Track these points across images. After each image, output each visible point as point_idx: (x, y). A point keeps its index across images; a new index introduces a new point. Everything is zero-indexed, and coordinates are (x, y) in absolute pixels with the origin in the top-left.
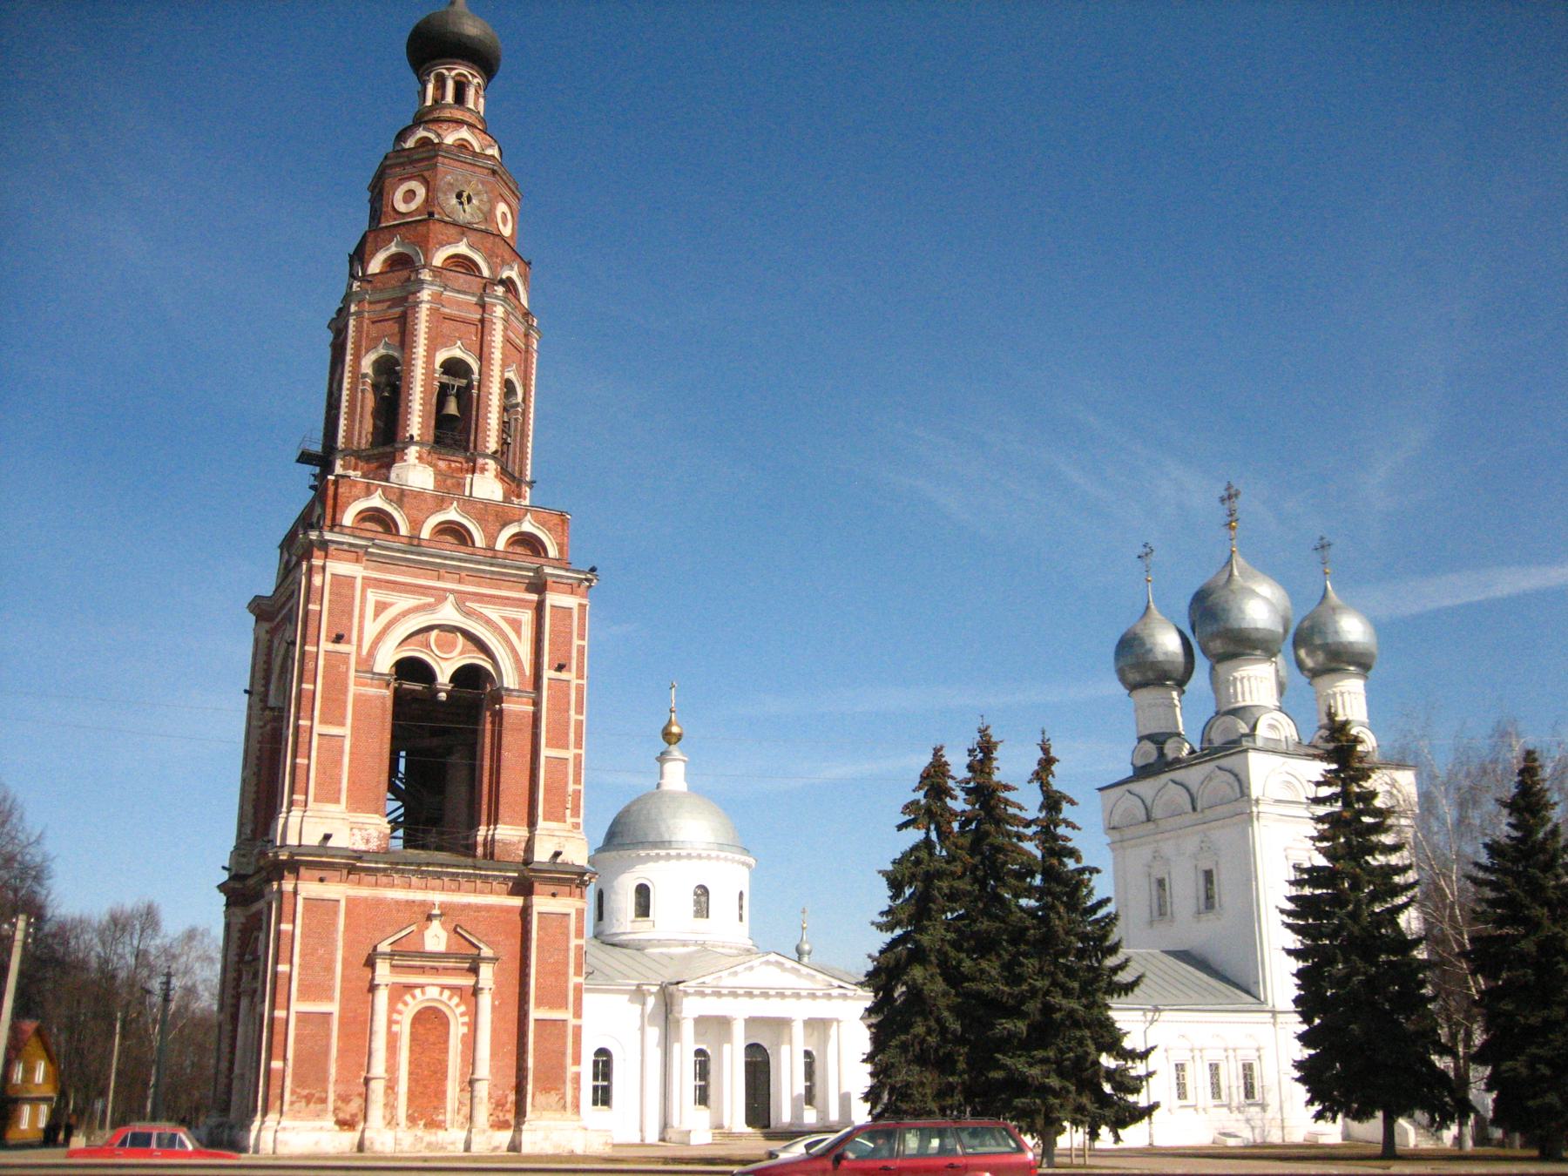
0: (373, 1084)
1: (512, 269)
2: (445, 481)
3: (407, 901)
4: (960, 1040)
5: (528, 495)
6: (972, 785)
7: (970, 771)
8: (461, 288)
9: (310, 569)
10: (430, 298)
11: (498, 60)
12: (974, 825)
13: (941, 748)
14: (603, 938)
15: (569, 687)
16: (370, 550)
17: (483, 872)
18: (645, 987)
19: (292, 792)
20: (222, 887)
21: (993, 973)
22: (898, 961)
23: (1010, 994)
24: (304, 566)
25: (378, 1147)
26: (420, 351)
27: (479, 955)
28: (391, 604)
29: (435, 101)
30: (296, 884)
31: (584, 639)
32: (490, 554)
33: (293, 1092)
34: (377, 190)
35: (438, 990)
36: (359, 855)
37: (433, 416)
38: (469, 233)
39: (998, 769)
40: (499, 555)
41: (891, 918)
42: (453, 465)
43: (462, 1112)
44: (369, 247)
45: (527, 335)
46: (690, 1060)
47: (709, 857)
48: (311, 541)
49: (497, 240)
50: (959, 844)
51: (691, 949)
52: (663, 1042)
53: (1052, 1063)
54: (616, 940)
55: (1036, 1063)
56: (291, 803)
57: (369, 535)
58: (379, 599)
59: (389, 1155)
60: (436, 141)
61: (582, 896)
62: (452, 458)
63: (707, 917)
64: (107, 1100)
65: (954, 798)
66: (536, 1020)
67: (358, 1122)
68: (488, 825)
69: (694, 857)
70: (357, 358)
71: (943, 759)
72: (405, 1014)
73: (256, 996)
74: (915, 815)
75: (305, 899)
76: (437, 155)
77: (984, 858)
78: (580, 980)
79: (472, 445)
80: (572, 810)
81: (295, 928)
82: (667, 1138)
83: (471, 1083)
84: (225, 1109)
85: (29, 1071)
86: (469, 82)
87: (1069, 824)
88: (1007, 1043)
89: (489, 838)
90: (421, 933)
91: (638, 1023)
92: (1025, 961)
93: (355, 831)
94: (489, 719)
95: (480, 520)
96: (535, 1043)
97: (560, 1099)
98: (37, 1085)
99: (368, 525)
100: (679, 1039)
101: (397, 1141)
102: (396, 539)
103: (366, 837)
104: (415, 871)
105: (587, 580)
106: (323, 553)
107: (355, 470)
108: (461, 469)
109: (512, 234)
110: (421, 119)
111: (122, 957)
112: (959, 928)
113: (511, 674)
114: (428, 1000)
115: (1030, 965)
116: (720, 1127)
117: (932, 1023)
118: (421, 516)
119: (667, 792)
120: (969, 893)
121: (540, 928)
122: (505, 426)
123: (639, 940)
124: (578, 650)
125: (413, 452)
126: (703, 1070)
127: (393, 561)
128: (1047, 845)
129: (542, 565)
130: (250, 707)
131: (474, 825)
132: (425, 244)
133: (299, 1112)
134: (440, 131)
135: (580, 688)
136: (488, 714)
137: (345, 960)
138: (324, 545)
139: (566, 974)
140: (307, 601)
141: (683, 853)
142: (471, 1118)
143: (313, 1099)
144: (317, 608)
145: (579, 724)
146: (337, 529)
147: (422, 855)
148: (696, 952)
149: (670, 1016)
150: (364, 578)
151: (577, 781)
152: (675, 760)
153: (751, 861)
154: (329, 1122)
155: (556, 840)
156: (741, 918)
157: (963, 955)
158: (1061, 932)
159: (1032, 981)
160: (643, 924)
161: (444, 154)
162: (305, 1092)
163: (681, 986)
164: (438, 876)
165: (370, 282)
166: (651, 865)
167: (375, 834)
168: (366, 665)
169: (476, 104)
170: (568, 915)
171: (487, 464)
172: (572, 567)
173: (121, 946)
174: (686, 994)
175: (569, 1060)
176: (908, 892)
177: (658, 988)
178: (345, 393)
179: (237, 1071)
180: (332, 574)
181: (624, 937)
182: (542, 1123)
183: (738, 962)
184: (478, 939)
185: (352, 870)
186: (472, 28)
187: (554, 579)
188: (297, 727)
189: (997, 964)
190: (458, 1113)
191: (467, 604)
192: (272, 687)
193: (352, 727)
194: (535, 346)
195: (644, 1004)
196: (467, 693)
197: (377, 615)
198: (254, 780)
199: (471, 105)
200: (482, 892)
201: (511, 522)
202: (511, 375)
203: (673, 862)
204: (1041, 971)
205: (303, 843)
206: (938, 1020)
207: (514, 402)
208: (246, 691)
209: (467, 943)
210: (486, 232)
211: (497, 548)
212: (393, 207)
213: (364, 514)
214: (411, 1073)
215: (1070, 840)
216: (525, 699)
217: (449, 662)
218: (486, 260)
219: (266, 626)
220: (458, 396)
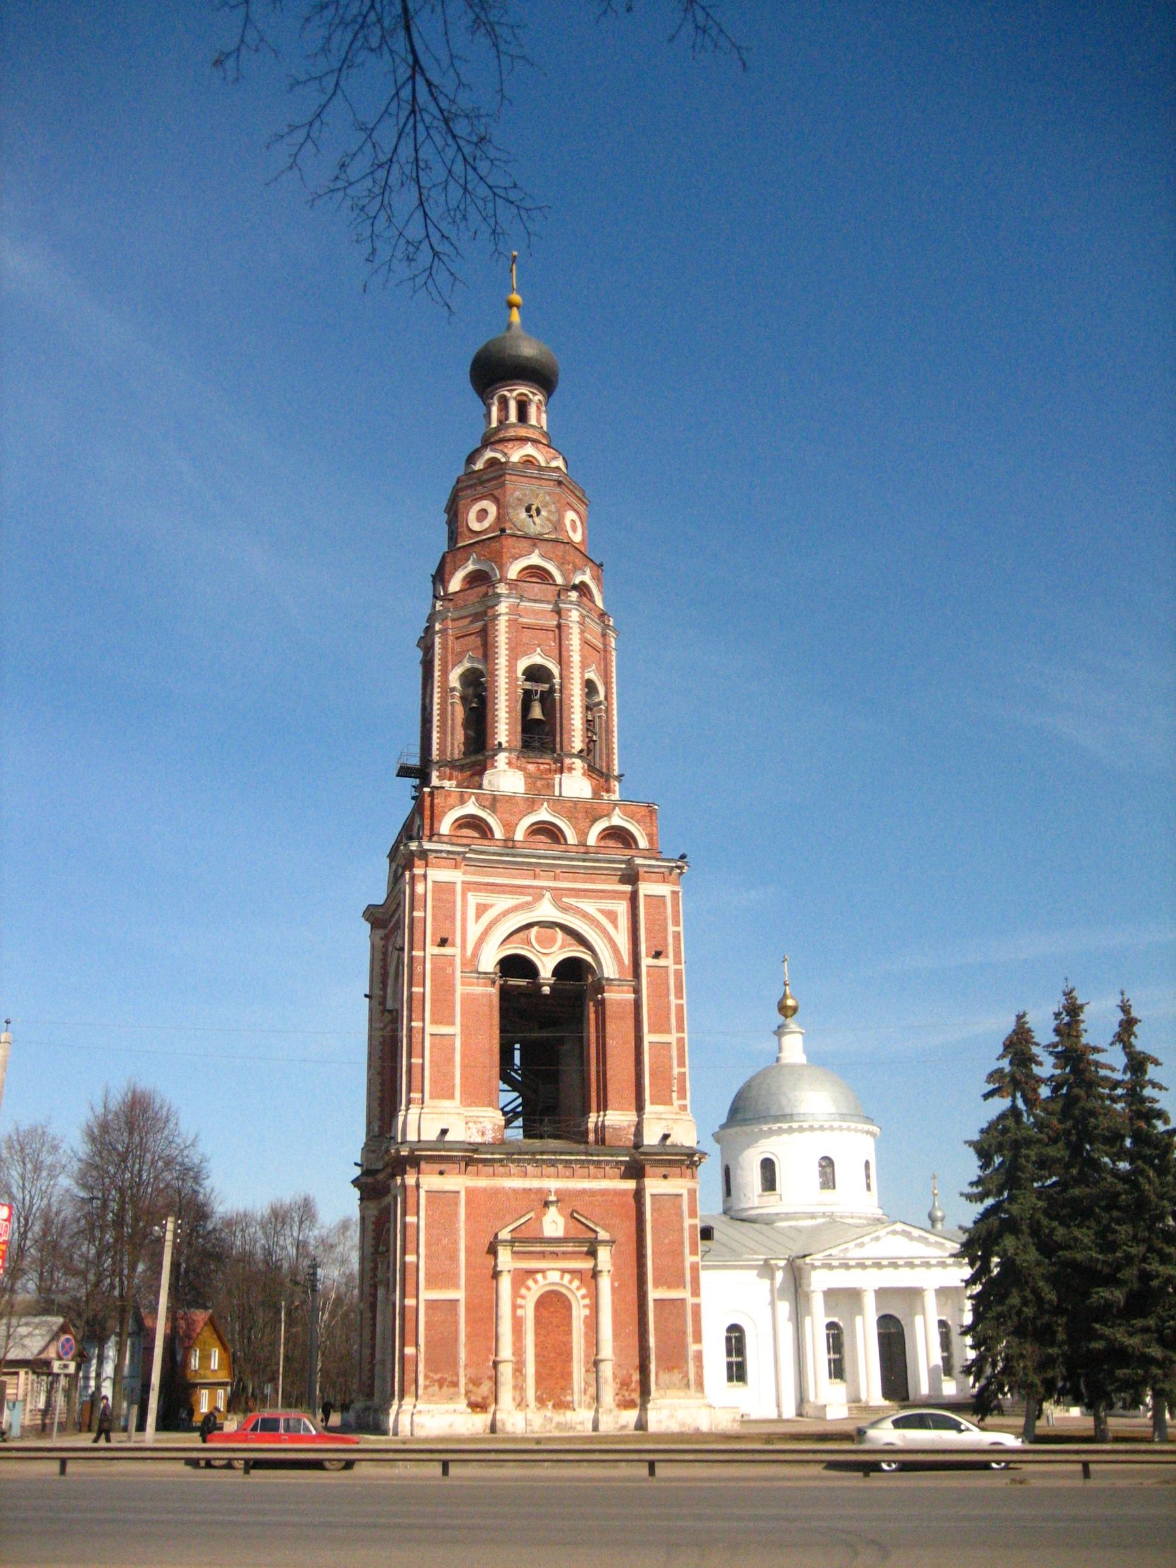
0: (502, 1367)
1: (584, 573)
2: (534, 783)
3: (524, 1190)
4: (1057, 1310)
5: (617, 788)
6: (1060, 1049)
7: (1057, 1035)
8: (537, 598)
9: (413, 877)
10: (507, 610)
11: (556, 375)
12: (1065, 1089)
13: (1024, 1015)
14: (732, 1213)
15: (667, 973)
16: (467, 855)
17: (595, 1158)
18: (772, 1262)
19: (409, 1091)
20: (356, 1182)
21: (1086, 1240)
22: (989, 1233)
23: (1104, 1262)
24: (407, 875)
25: (509, 1428)
26: (502, 661)
27: (596, 1238)
28: (491, 906)
29: (500, 422)
30: (418, 1178)
31: (678, 925)
32: (582, 849)
33: (426, 1377)
34: (452, 513)
35: (558, 1274)
36: (475, 1148)
37: (519, 722)
38: (540, 544)
39: (1086, 1031)
40: (591, 850)
41: (982, 1188)
42: (542, 767)
43: (589, 1393)
44: (448, 568)
45: (604, 635)
46: (822, 1334)
47: (831, 1128)
48: (412, 852)
49: (568, 547)
50: (1050, 1110)
51: (820, 1221)
52: (794, 1316)
53: (1152, 1332)
54: (744, 1215)
55: (1135, 1333)
56: (409, 1102)
57: (465, 841)
58: (479, 901)
59: (520, 1436)
60: (503, 460)
61: (693, 1177)
62: (540, 761)
63: (834, 1188)
64: (277, 1384)
65: (1040, 1064)
66: (655, 1300)
67: (489, 1405)
68: (598, 1111)
69: (816, 1129)
70: (445, 673)
71: (1027, 1026)
72: (528, 1299)
73: (390, 1287)
74: (1000, 1084)
75: (426, 1192)
76: (503, 475)
77: (1077, 1122)
78: (697, 1259)
79: (558, 746)
80: (678, 1092)
81: (419, 1220)
82: (804, 1413)
83: (596, 1363)
84: (370, 1395)
85: (205, 1358)
86: (530, 400)
87: (1155, 1085)
88: (1104, 1313)
89: (600, 1124)
90: (539, 1219)
91: (768, 1298)
92: (1117, 1228)
93: (471, 1125)
94: (592, 1009)
95: (571, 818)
96: (655, 1322)
97: (683, 1377)
98: (214, 1371)
99: (466, 832)
100: (809, 1312)
101: (527, 1422)
102: (492, 843)
103: (481, 1129)
104: (531, 1159)
105: (678, 867)
106: (424, 862)
107: (450, 779)
108: (550, 770)
109: (583, 540)
110: (489, 441)
111: (283, 1248)
112: (1052, 1196)
113: (610, 965)
114: (550, 1284)
115: (1123, 1232)
116: (858, 1400)
117: (1030, 1296)
118: (513, 819)
119: (787, 1066)
120: (1059, 1160)
121: (653, 1210)
122: (589, 725)
123: (768, 1214)
124: (674, 937)
125: (502, 758)
126: (836, 1338)
127: (490, 865)
128: (1134, 1108)
129: (633, 857)
130: (371, 1010)
131: (586, 1112)
132: (498, 559)
133: (433, 1395)
134: (506, 451)
135: (678, 973)
136: (591, 1004)
137: (467, 1248)
138: (424, 854)
139: (682, 1254)
140: (412, 909)
141: (805, 1125)
142: (597, 1398)
143: (445, 1383)
144: (421, 914)
145: (680, 1008)
146: (435, 838)
147: (537, 1143)
148: (824, 1224)
149: (799, 1290)
150: (463, 882)
151: (681, 1064)
152: (794, 1032)
153: (875, 1129)
154: (462, 1404)
155: (664, 1123)
156: (868, 1187)
157: (1055, 1224)
158: (1153, 1197)
159: (1125, 1247)
160: (771, 1198)
161: (510, 472)
162: (438, 1376)
163: (808, 1260)
164: (553, 1163)
165: (451, 600)
166: (774, 1139)
167: (489, 1126)
168: (471, 965)
169: (538, 420)
170: (680, 1195)
171: (573, 763)
172: (663, 856)
173: (282, 1238)
174: (814, 1267)
175: (690, 1339)
176: (998, 1160)
177: (785, 1262)
178: (436, 707)
179: (378, 1356)
180: (434, 882)
181: (753, 1212)
182: (666, 1401)
183: (865, 1233)
184: (594, 1222)
185: (469, 1162)
186: (528, 349)
187: (646, 869)
188: (410, 1029)
189: (1091, 1232)
190: (585, 1393)
191: (564, 900)
192: (389, 991)
193: (462, 1026)
194: (613, 645)
195: (772, 1278)
196: (570, 984)
197: (478, 917)
198: (378, 1080)
199: (533, 421)
200: (595, 1177)
201: (601, 817)
202: (591, 675)
203: (796, 1134)
204: (1135, 1238)
205: (422, 1138)
206: (1034, 1291)
207: (597, 700)
208: (366, 996)
209: (584, 1228)
210: (556, 541)
211: (588, 844)
212: (468, 526)
213: (460, 822)
214: (537, 1355)
215: (1158, 1101)
216: (625, 988)
217: (550, 958)
218: (558, 568)
219: (381, 933)
220: (543, 700)
